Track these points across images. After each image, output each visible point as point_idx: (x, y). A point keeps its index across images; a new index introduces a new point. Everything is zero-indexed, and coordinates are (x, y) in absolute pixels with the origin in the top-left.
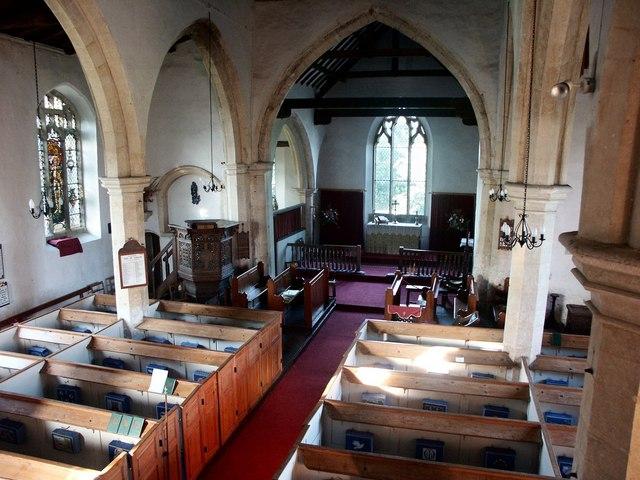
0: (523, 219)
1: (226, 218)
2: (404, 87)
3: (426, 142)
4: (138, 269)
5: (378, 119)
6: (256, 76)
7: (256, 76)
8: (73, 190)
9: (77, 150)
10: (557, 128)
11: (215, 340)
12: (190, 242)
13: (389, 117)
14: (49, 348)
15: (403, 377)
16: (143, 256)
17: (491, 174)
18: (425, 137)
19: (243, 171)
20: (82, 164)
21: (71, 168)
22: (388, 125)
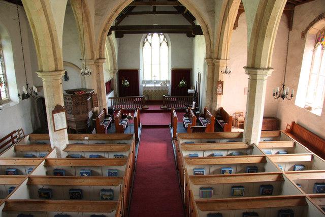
1: (84, 88)
2: (155, 20)
3: (168, 45)
4: (62, 120)
5: (145, 35)
10: (313, 49)
11: (107, 152)
14: (19, 168)
16: (64, 113)
20: (4, 64)
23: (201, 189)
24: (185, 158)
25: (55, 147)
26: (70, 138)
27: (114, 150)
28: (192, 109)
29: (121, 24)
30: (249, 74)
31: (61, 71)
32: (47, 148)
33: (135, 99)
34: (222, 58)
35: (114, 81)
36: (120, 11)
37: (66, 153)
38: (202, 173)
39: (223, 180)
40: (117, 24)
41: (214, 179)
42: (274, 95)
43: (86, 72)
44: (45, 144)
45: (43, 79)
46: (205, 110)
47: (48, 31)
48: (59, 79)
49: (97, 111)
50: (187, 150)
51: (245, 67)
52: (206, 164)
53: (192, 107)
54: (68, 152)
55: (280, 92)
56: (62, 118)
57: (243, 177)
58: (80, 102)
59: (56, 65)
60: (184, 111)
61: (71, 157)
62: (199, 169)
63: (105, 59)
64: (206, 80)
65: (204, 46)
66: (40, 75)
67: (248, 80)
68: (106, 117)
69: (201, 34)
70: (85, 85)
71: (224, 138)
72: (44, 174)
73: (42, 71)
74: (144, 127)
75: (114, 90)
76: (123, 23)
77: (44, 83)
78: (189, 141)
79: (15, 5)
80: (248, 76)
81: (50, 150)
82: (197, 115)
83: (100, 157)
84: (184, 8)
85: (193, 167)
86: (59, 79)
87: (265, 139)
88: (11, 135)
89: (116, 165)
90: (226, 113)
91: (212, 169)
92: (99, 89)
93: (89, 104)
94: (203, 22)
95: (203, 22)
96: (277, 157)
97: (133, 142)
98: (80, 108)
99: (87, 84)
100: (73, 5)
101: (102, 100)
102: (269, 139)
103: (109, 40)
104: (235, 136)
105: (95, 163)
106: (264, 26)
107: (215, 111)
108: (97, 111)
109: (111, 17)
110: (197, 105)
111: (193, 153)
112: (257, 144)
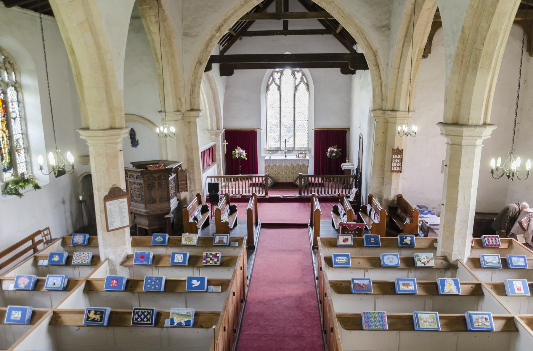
3: (308, 88)
4: (121, 212)
5: (269, 71)
6: (186, 35)
7: (186, 35)
8: (17, 140)
9: (19, 102)
12: (141, 181)
13: (278, 70)
18: (307, 85)
19: (180, 117)
21: (14, 119)
22: (277, 76)
25: (107, 259)
26: (135, 244)
29: (230, 52)
30: (447, 135)
33: (251, 178)
34: (402, 108)
35: (217, 149)
36: (225, 31)
40: (222, 52)
42: (492, 172)
45: (90, 142)
48: (117, 143)
49: (185, 199)
56: (121, 208)
58: (156, 182)
63: (199, 110)
64: (372, 145)
65: (370, 89)
66: (83, 134)
70: (167, 154)
74: (265, 226)
76: (233, 51)
77: (91, 149)
78: (320, 309)
79: (37, 15)
80: (445, 139)
84: (336, 23)
86: (117, 143)
88: (32, 237)
92: (190, 161)
93: (172, 185)
94: (369, 46)
95: (369, 46)
97: (243, 251)
98: (156, 193)
99: (169, 152)
100: (145, 18)
103: (209, 79)
106: (476, 49)
107: (387, 200)
108: (185, 199)
109: (211, 39)
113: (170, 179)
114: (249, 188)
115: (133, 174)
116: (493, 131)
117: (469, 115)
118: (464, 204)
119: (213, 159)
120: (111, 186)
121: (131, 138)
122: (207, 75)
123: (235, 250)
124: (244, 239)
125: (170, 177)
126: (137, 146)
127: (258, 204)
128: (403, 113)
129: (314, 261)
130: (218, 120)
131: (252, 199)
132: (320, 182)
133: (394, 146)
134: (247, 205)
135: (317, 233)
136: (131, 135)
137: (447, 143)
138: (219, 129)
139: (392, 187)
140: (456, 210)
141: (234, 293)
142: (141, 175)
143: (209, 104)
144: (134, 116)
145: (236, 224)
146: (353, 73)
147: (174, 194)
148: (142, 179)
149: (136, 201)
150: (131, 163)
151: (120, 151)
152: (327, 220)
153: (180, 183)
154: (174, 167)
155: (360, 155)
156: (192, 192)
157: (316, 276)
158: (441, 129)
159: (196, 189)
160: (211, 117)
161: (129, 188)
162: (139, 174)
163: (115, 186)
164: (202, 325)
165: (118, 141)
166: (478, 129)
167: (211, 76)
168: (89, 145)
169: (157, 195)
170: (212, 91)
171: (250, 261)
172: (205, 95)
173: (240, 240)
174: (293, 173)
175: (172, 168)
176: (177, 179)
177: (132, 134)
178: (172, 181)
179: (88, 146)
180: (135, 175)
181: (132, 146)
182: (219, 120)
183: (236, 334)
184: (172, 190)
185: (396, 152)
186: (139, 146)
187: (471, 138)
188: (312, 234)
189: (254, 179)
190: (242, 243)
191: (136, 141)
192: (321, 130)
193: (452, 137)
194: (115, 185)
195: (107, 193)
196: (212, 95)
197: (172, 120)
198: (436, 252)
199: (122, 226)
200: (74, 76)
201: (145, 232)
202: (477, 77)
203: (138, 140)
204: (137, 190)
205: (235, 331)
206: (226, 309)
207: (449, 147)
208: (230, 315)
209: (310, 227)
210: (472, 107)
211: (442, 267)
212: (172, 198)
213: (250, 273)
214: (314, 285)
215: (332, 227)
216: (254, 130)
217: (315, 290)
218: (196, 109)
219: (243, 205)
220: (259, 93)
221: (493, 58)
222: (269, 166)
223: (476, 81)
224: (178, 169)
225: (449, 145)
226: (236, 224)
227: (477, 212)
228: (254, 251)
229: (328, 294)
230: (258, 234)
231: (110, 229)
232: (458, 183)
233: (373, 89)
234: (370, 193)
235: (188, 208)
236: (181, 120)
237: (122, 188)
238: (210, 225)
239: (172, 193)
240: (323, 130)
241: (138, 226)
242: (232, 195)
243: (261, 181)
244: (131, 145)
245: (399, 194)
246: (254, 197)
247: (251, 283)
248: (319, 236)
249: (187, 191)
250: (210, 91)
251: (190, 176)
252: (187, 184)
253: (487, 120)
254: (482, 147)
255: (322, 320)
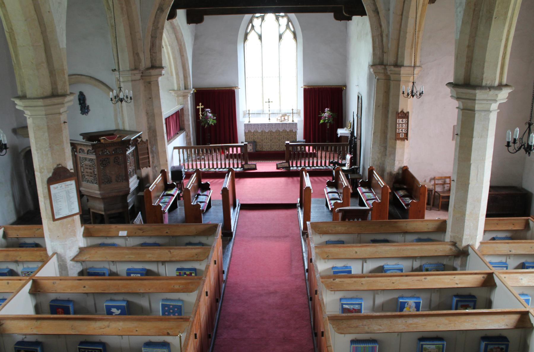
0: (120, 90)
1: (121, 127)
3: (295, 37)
4: (69, 198)
5: (247, 17)
11: (163, 262)
12: (93, 157)
13: (258, 15)
15: (134, 196)
17: (385, 69)
18: (294, 34)
19: (138, 77)
23: (353, 342)
24: (322, 277)
26: (87, 234)
27: (177, 259)
28: (343, 171)
30: (458, 98)
31: (64, 95)
32: (38, 253)
33: (227, 148)
34: (406, 63)
35: (185, 113)
37: (79, 264)
38: (357, 307)
39: (400, 325)
41: (380, 321)
42: (508, 145)
43: (121, 96)
44: (37, 245)
45: (27, 113)
46: (371, 171)
47: (33, 12)
48: (60, 114)
49: (147, 177)
50: (327, 258)
51: (449, 84)
52: (366, 288)
53: (344, 165)
54: (82, 262)
55: (521, 139)
56: (68, 192)
57: (443, 320)
59: (54, 84)
60: (326, 173)
61: (89, 274)
62: (352, 299)
64: (373, 106)
66: (20, 105)
67: (457, 111)
68: (168, 187)
69: (362, 13)
70: (123, 123)
71: (406, 233)
72: (30, 311)
73: (23, 97)
74: (245, 207)
75: (185, 131)
80: (456, 103)
81: (45, 260)
82: (354, 183)
83: (149, 273)
85: (339, 295)
86: (60, 114)
87: (494, 235)
89: (178, 291)
90: (413, 178)
91: (380, 300)
92: (153, 131)
93: (131, 161)
96: (519, 276)
97: (218, 239)
101: (158, 153)
102: (508, 234)
104: (431, 227)
105: (135, 286)
107: (390, 174)
108: (147, 177)
110: (354, 161)
111: (340, 264)
112: (477, 246)
113: (128, 153)
114: (225, 161)
115: (83, 148)
116: (509, 93)
117: (483, 74)
118: (477, 180)
119: (181, 128)
120: (55, 166)
121: (80, 104)
122: (171, 23)
123: (208, 239)
124: (219, 226)
125: (127, 150)
126: (87, 113)
127: (236, 180)
128: (407, 69)
129: (304, 250)
130: (185, 77)
131: (228, 176)
132: (311, 151)
133: (398, 109)
134: (222, 183)
135: (307, 217)
136: (80, 100)
137: (457, 108)
138: (188, 89)
139: (396, 158)
140: (468, 187)
141: (207, 292)
142: (93, 149)
143: (174, 58)
144: (83, 77)
145: (209, 206)
146: (350, 19)
147: (133, 171)
148: (94, 153)
149: (88, 181)
150: (81, 135)
151: (65, 122)
152: (320, 199)
153: (140, 157)
154: (132, 139)
155: (359, 118)
156: (155, 167)
157: (306, 268)
158: (451, 90)
159: (160, 164)
160: (177, 74)
161: (79, 166)
162: (91, 149)
163: (60, 166)
164: (170, 332)
165: (62, 110)
166: (492, 92)
167: (176, 24)
168: (28, 117)
169: (113, 173)
170: (178, 43)
171: (228, 251)
172: (169, 47)
173: (211, 230)
174: (279, 140)
175: (130, 140)
176: (136, 153)
177: (82, 99)
178: (130, 156)
179: (26, 118)
180: (86, 149)
181: (81, 113)
182: (187, 78)
183: (210, 339)
184: (130, 166)
185: (400, 115)
186: (90, 113)
187: (485, 102)
188: (302, 217)
189: (231, 149)
190: (216, 230)
191: (86, 108)
192: (311, 88)
193: (463, 101)
194: (59, 165)
195: (51, 175)
196: (178, 48)
197: (128, 81)
198: (445, 235)
199: (70, 214)
200: (6, 33)
201: (99, 219)
202: (492, 29)
203: (88, 106)
204: (88, 167)
205: (209, 336)
206: (197, 313)
207: (461, 112)
208: (202, 319)
209: (299, 208)
210: (486, 65)
211: (451, 254)
212: (131, 177)
213: (227, 266)
214: (304, 278)
215: (325, 207)
216: (230, 89)
217: (305, 284)
218: (157, 66)
219: (218, 181)
220: (235, 43)
221: (509, 6)
222: (249, 132)
223: (490, 34)
224: (138, 140)
225: (460, 110)
226: (209, 206)
227: (495, 184)
228: (232, 238)
229: (318, 292)
230: (237, 218)
231: (56, 217)
232: (471, 155)
233: (373, 40)
234: (370, 166)
235: (151, 189)
236: (140, 80)
237: (69, 168)
238: (179, 207)
239: (130, 170)
240: (314, 88)
241: (92, 210)
242: (205, 169)
243: (239, 152)
244: (80, 112)
245: (404, 166)
246: (230, 173)
247: (229, 277)
248: (309, 220)
249: (150, 166)
250: (175, 43)
251: (153, 149)
252: (149, 157)
253: (503, 80)
254: (498, 113)
255: (312, 320)
